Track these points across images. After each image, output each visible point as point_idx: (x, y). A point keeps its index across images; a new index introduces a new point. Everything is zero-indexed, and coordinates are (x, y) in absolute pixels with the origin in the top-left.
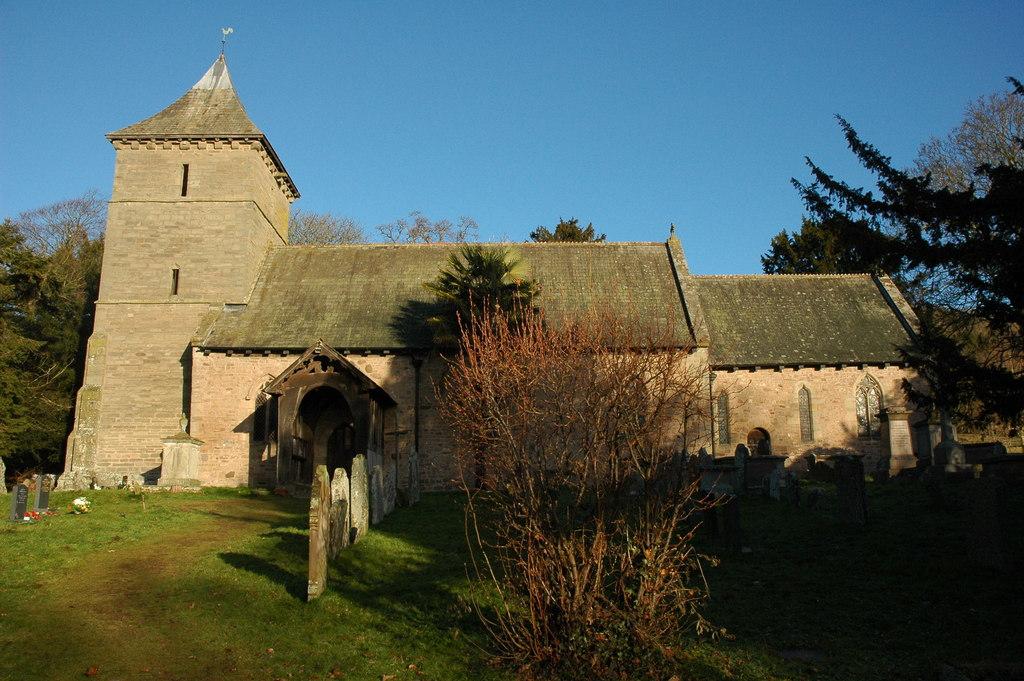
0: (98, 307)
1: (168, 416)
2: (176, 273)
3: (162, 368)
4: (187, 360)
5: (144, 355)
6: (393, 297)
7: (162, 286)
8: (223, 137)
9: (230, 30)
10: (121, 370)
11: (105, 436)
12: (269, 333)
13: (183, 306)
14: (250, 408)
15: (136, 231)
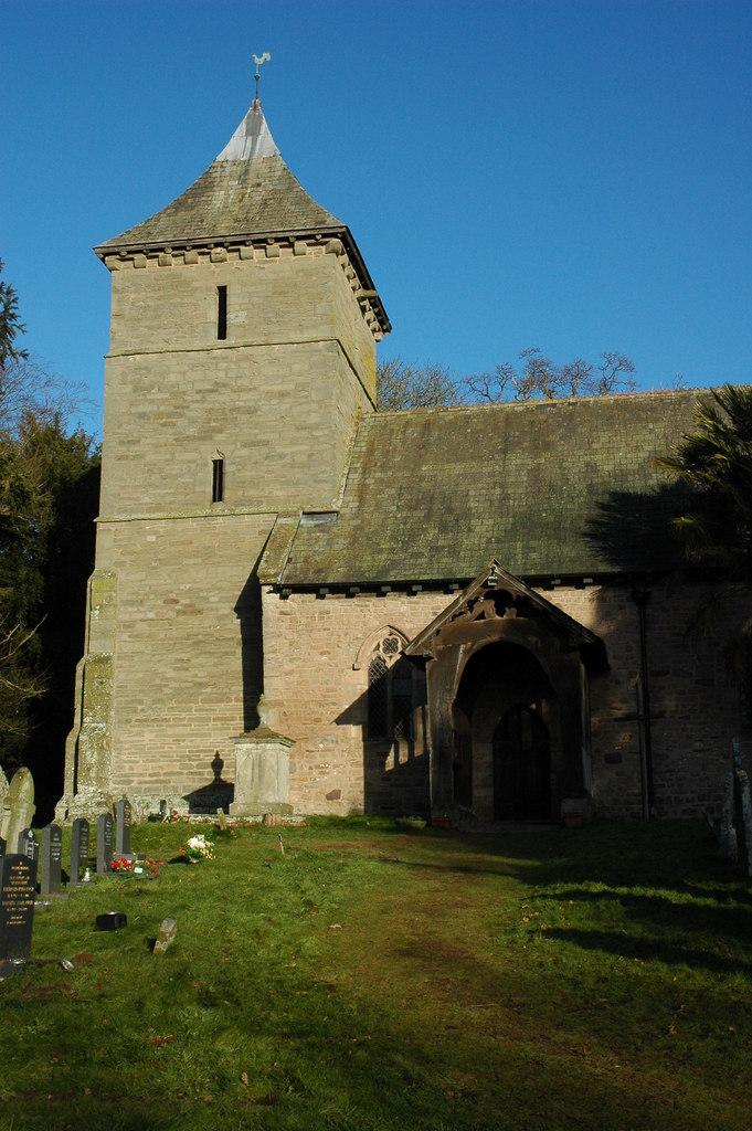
0: (100, 527)
1: (221, 701)
2: (219, 466)
3: (207, 623)
4: (249, 608)
5: (176, 602)
6: (582, 486)
7: (197, 489)
8: (281, 235)
9: (266, 56)
10: (142, 627)
11: (119, 734)
12: (384, 556)
13: (234, 519)
14: (360, 683)
15: (152, 402)
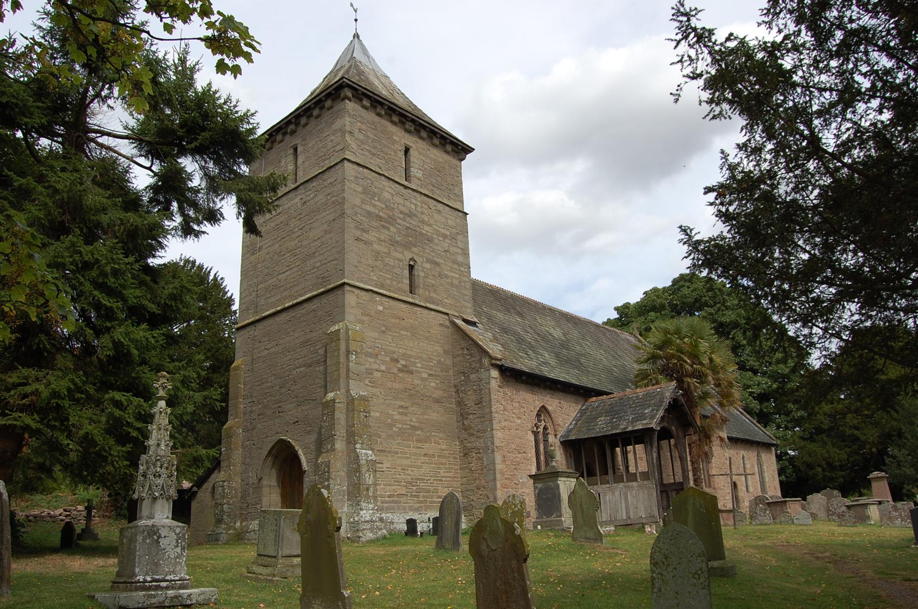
15: (374, 206)
